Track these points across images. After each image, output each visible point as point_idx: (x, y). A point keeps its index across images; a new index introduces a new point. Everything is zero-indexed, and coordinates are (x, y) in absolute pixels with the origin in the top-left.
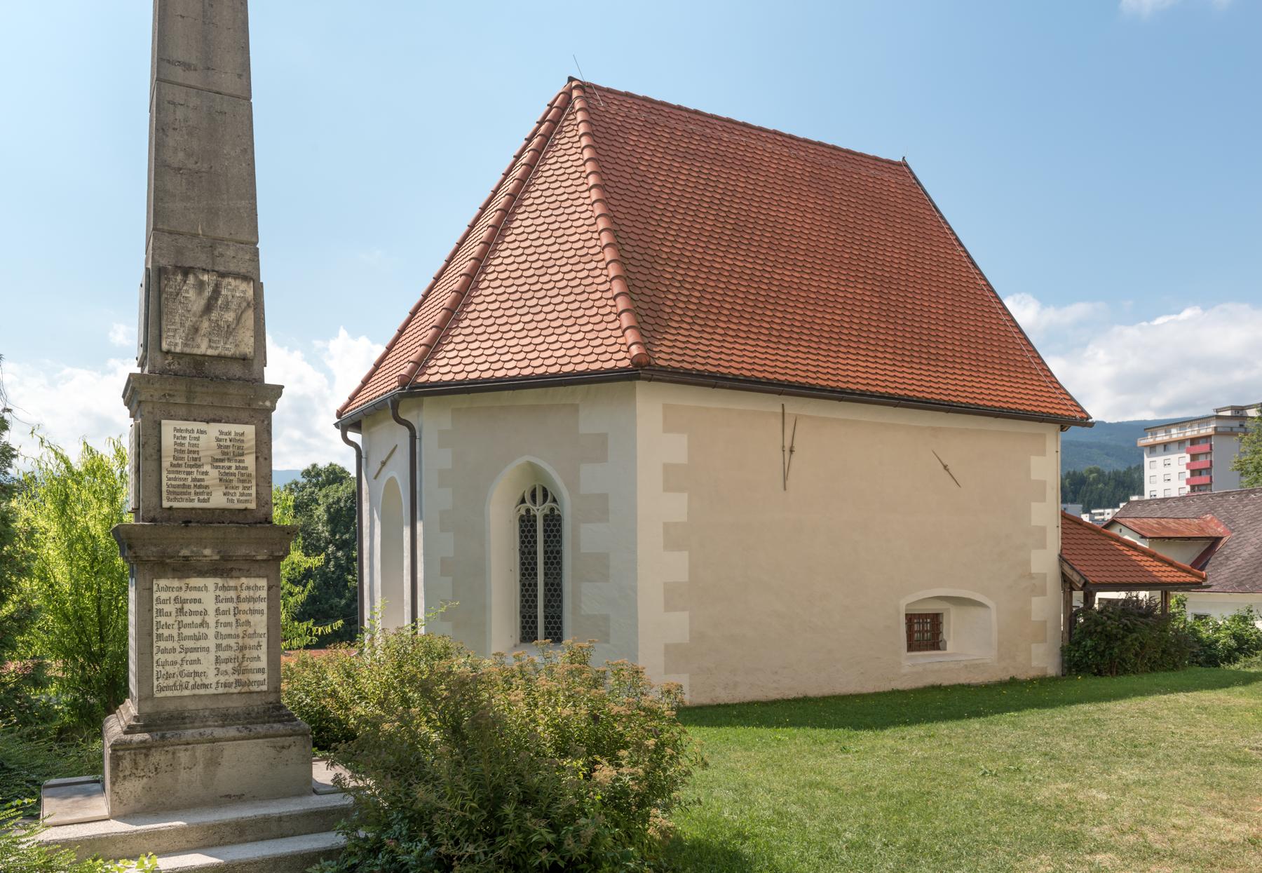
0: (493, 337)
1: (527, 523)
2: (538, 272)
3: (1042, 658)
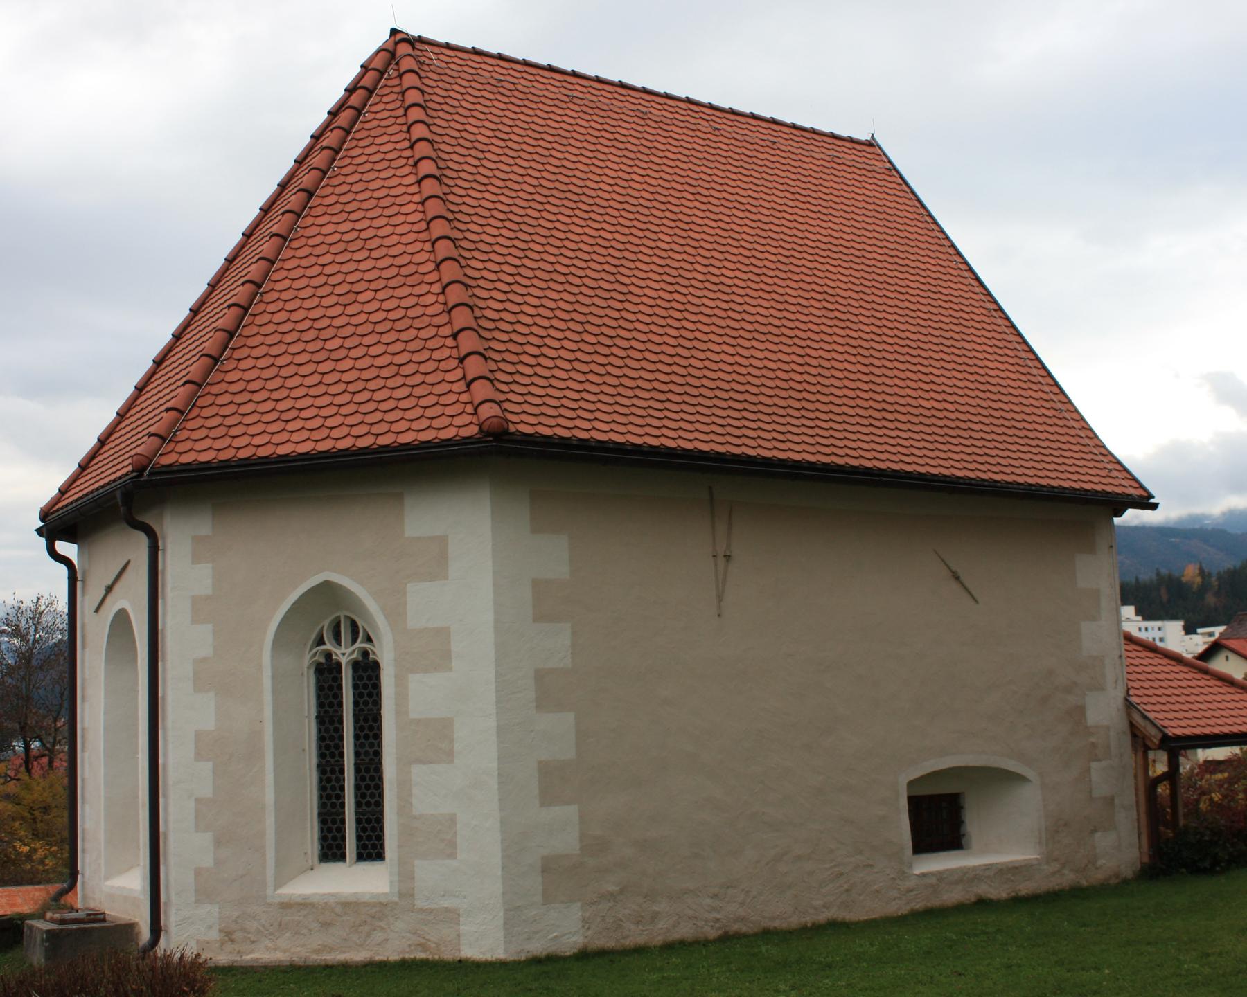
0: (275, 395)
1: (327, 672)
2: (343, 300)
3: (1119, 847)
